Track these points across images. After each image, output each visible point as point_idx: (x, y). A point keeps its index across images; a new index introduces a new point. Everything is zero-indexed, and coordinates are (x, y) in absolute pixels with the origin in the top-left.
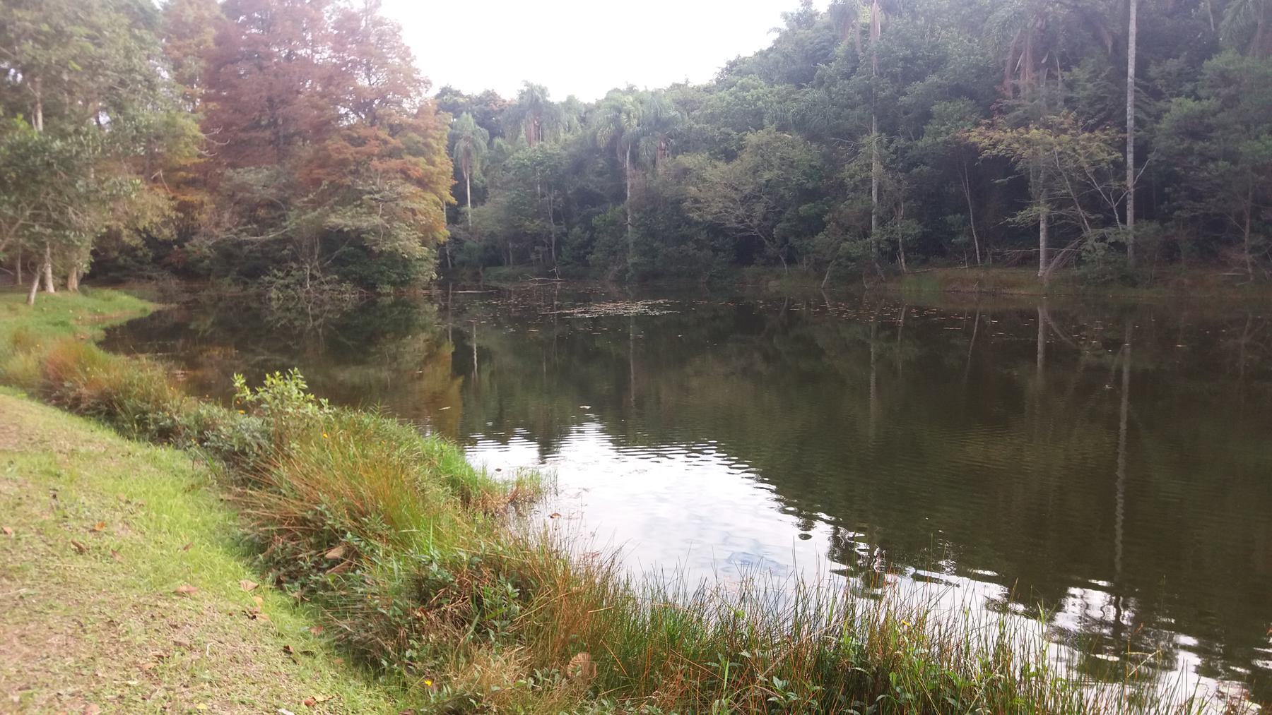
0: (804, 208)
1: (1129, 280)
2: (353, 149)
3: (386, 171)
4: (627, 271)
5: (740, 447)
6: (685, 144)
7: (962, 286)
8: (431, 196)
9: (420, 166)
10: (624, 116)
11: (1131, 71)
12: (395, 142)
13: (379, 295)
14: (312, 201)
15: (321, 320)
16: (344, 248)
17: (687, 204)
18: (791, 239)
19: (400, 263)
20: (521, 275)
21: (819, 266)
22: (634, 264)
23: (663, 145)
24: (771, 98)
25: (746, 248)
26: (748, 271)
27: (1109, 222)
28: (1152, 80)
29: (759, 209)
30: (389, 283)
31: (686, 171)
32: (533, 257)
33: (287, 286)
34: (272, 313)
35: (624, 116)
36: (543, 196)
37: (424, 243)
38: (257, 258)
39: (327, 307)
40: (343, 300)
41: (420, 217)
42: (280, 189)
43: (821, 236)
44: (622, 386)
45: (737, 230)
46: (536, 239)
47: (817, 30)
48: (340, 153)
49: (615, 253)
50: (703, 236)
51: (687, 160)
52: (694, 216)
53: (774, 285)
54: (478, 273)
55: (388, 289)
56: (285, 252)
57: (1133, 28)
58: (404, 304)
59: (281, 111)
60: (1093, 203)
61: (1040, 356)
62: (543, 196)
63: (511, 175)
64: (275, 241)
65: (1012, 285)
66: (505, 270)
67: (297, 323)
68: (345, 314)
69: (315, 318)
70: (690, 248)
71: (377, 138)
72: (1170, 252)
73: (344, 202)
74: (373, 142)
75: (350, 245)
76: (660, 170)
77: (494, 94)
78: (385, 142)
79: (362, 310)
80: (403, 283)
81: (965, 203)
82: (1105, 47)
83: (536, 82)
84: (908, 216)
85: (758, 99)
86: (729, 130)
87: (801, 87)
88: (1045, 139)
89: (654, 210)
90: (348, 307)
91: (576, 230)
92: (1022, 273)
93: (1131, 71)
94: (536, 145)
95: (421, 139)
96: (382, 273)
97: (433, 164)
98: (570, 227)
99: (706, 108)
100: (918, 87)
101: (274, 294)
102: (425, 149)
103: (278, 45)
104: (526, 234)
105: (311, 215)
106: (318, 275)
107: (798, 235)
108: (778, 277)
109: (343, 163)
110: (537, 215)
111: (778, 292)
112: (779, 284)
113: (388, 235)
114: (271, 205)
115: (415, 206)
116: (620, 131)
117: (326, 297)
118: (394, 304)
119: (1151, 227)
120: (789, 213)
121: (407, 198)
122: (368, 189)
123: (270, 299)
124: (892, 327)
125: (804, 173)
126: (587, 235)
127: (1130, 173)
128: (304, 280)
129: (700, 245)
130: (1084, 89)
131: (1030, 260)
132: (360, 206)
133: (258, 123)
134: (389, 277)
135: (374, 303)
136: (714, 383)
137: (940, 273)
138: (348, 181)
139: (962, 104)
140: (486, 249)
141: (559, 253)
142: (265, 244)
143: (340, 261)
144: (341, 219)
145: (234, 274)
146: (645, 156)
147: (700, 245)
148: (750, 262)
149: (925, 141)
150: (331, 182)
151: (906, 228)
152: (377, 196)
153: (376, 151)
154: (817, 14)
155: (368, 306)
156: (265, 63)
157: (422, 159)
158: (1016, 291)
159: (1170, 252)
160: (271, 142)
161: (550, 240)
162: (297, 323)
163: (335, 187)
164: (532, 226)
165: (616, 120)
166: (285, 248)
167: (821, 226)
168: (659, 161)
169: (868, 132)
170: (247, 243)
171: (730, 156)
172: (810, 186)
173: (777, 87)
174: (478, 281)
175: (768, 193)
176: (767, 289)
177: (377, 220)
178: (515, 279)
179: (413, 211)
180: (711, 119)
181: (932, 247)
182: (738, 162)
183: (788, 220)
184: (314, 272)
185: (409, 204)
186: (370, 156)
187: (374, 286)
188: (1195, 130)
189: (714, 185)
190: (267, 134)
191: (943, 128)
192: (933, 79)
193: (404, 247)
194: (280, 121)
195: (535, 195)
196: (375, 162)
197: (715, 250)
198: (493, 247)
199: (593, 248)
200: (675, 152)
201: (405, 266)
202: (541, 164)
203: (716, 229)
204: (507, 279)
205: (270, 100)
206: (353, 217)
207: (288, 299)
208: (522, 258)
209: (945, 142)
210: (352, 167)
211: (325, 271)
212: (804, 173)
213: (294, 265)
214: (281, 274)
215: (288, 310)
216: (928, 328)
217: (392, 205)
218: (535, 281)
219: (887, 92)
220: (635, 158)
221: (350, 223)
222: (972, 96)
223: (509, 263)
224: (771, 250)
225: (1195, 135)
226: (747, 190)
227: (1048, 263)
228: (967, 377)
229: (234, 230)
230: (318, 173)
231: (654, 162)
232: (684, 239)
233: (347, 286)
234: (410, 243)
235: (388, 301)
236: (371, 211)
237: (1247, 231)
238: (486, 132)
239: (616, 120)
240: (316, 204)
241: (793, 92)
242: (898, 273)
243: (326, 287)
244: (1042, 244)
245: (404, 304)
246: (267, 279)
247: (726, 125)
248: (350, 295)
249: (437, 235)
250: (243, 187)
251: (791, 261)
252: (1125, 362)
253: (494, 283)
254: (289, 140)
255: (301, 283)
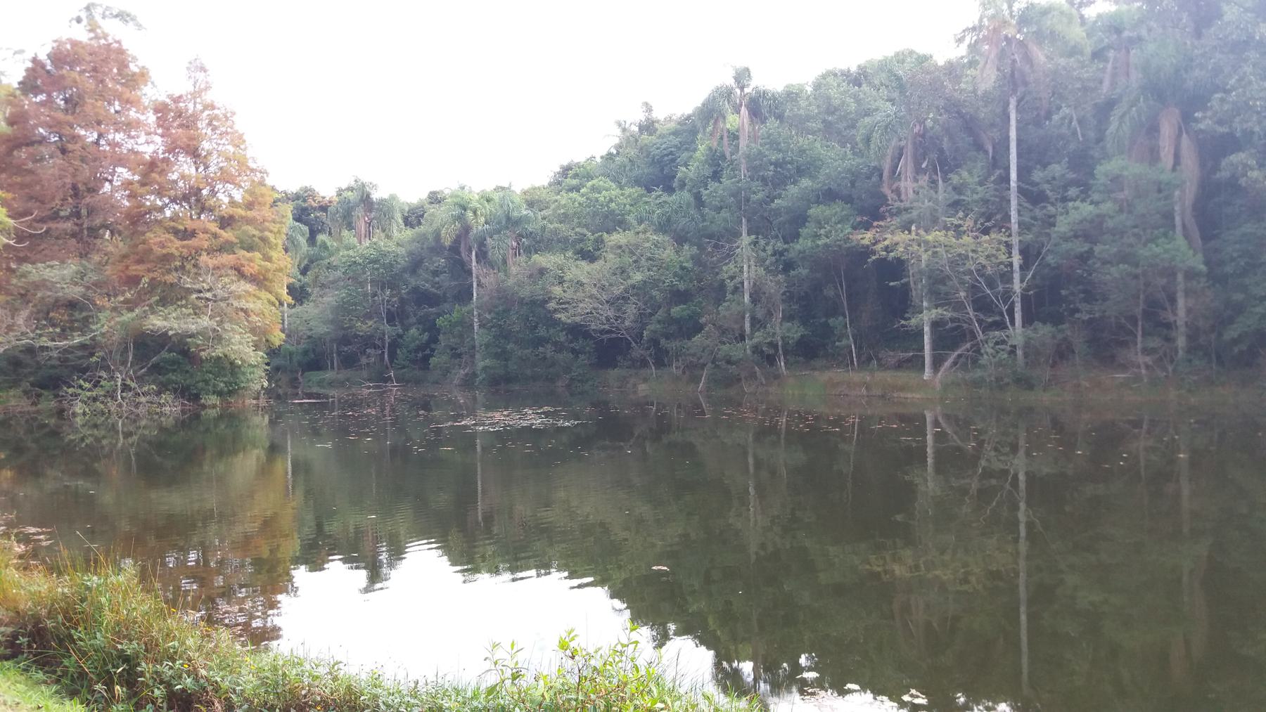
0: (676, 311)
1: (1025, 383)
2: (178, 243)
3: (217, 268)
4: (475, 375)
5: (590, 557)
6: (537, 243)
7: (843, 391)
8: (265, 295)
9: (254, 262)
10: (470, 214)
11: (1013, 175)
12: (227, 235)
13: (204, 407)
14: (126, 301)
15: (135, 438)
16: (164, 354)
17: (552, 305)
18: (663, 341)
19: (228, 368)
20: (348, 380)
21: (693, 370)
22: (485, 368)
23: (515, 244)
24: (622, 200)
25: (608, 349)
26: (613, 373)
27: (1000, 326)
28: (1038, 184)
29: (631, 310)
30: (214, 393)
31: (542, 272)
32: (364, 360)
33: (95, 399)
34: (76, 431)
35: (470, 214)
36: (375, 295)
37: (257, 347)
38: (53, 367)
39: (143, 423)
40: (161, 414)
41: (254, 318)
42: (88, 288)
43: (697, 339)
44: (466, 498)
45: (602, 332)
46: (368, 342)
47: (661, 136)
48: (163, 247)
49: (459, 356)
50: (562, 337)
51: (541, 260)
52: (562, 317)
53: (643, 388)
54: (297, 379)
55: (213, 399)
56: (94, 359)
57: (1013, 134)
58: (232, 417)
59: (88, 200)
60: (983, 305)
61: (930, 461)
62: (375, 295)
63: (339, 273)
64: (83, 346)
65: (902, 389)
66: (329, 375)
67: (104, 442)
68: (162, 429)
69: (128, 435)
70: (548, 350)
71: (205, 231)
72: (1062, 353)
73: (164, 302)
74: (201, 235)
75: (170, 351)
76: (514, 270)
77: (312, 190)
78: (215, 236)
79: (182, 424)
80: (232, 391)
81: (852, 304)
82: (986, 152)
83: (365, 179)
84: (788, 318)
85: (611, 200)
86: (585, 231)
87: (649, 191)
88: (926, 238)
89: (507, 311)
90: (168, 422)
91: (413, 331)
92: (903, 377)
93: (1013, 175)
94: (367, 243)
95: (257, 233)
96: (206, 382)
97: (269, 259)
98: (406, 329)
99: (558, 207)
100: (793, 190)
101: (79, 408)
102: (262, 244)
103: (86, 127)
104: (356, 336)
105: (127, 317)
106: (133, 385)
107: (668, 337)
108: (645, 380)
109: (167, 258)
110: (369, 316)
111: (645, 397)
112: (649, 387)
113: (219, 339)
114: (72, 305)
115: (251, 306)
116: (467, 229)
117: (141, 410)
118: (221, 417)
119: (1044, 331)
120: (661, 314)
121: (239, 297)
122: (197, 286)
123: (74, 415)
124: (773, 429)
125: (675, 275)
126: (426, 336)
127: (1017, 276)
128: (115, 391)
129: (559, 347)
130: (974, 191)
131: (916, 363)
132: (185, 306)
133: (57, 213)
134: (214, 386)
135: (197, 416)
136: (584, 496)
137: (826, 376)
138: (171, 278)
139: (837, 209)
140: (306, 352)
141: (393, 355)
142: (66, 351)
143: (157, 369)
144: (161, 321)
145: (26, 385)
146: (495, 255)
147: (559, 347)
148: (613, 364)
149: (803, 244)
150: (153, 279)
151: (783, 330)
152: (209, 295)
153: (206, 245)
154: (658, 121)
155: (191, 420)
156: (70, 147)
157: (257, 255)
158: (909, 395)
159: (1062, 353)
160: (74, 235)
161: (382, 339)
162: (104, 442)
163: (153, 284)
164: (364, 327)
165: (460, 218)
166: (92, 355)
167: (699, 328)
168: (510, 262)
169: (738, 235)
170: (43, 348)
171: (589, 256)
172: (682, 287)
173: (628, 191)
174: (296, 388)
175: (636, 294)
176: (635, 392)
177: (205, 322)
178: (341, 384)
179: (245, 311)
180: (564, 218)
181: (810, 351)
182: (601, 262)
183: (659, 322)
184: (128, 382)
185: (243, 304)
186: (198, 251)
187: (196, 398)
188: (1091, 232)
189: (578, 287)
190: (69, 225)
191: (822, 231)
192: (806, 182)
193: (235, 352)
194: (84, 212)
195: (365, 295)
196: (204, 258)
197: (573, 351)
198: (314, 350)
199: (433, 350)
200: (529, 251)
201: (233, 373)
202: (375, 261)
203: (577, 331)
204: (331, 384)
205: (74, 187)
206: (177, 318)
207: (95, 413)
208: (349, 361)
209: (826, 245)
210: (178, 264)
211: (140, 380)
212: (675, 275)
213: (104, 374)
214: (87, 385)
215: (96, 426)
216: (815, 436)
217: (223, 305)
218: (369, 388)
219: (760, 195)
220: (482, 255)
221: (176, 326)
222: (848, 200)
223: (332, 368)
224: (637, 352)
225: (1087, 237)
226: (617, 291)
227: (937, 363)
228: (860, 485)
229: (32, 335)
230: (136, 269)
231: (505, 262)
232: (541, 342)
233: (166, 397)
234: (242, 348)
235: (213, 413)
236: (197, 312)
237: (1140, 333)
238: (306, 229)
239: (460, 218)
240: (130, 305)
241: (642, 196)
242: (777, 377)
243: (143, 399)
244: (927, 348)
245: (231, 418)
246: (71, 391)
247: (579, 225)
248: (171, 407)
249: (272, 339)
250: (42, 284)
251: (660, 363)
252: (1019, 465)
253: (315, 390)
254: (94, 232)
255: (111, 395)
